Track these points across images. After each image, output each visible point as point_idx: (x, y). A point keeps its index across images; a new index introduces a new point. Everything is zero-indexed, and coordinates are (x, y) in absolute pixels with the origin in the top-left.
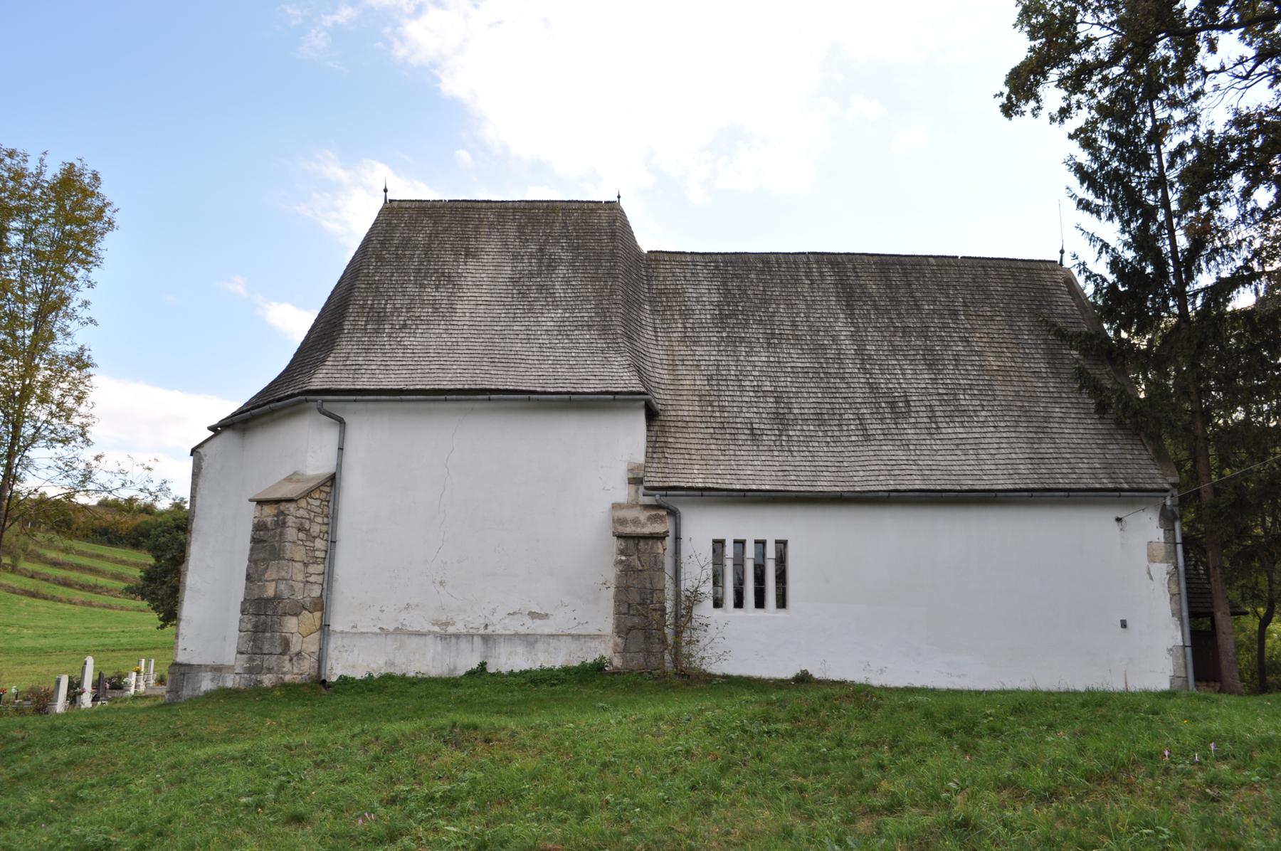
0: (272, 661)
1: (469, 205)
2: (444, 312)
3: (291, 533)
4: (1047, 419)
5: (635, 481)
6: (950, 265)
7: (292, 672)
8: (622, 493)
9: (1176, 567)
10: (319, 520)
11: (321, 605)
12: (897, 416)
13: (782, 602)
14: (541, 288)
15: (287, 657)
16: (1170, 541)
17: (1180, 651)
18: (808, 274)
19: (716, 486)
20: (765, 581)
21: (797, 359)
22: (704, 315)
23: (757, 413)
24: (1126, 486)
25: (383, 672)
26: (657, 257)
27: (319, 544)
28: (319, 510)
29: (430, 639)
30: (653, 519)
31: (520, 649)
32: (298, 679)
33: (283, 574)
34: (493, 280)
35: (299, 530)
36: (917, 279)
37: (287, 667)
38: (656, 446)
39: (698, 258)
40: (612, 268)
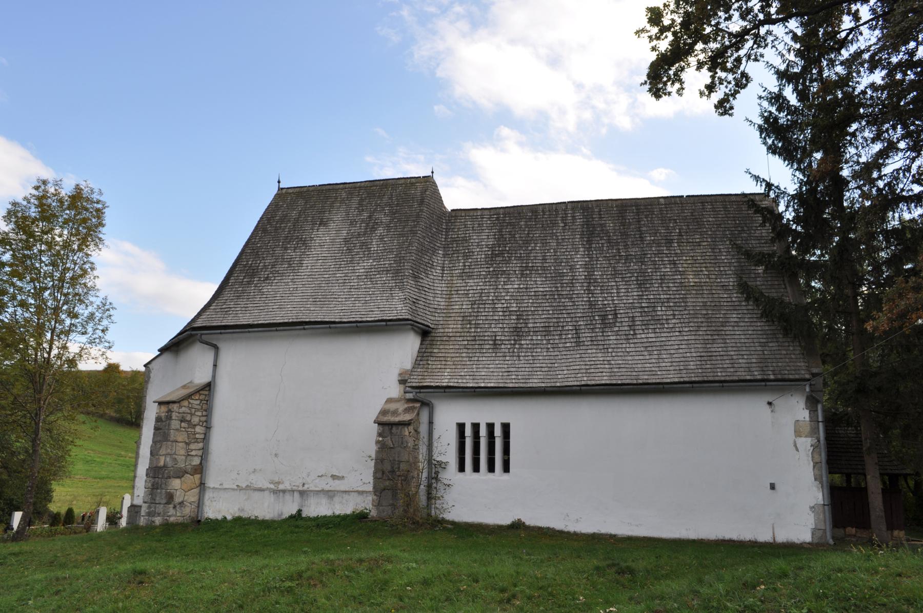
0: (160, 508)
1: (330, 187)
2: (294, 266)
3: (175, 424)
4: (724, 324)
5: (402, 382)
6: (675, 203)
7: (176, 516)
8: (395, 391)
9: (819, 441)
10: (199, 414)
11: (200, 470)
12: (606, 324)
13: (506, 468)
14: (363, 244)
15: (171, 506)
17: (821, 509)
18: (564, 219)
19: (456, 385)
20: (488, 450)
21: (540, 284)
23: (499, 329)
24: (772, 377)
25: (237, 515)
26: (458, 213)
27: (199, 429)
28: (199, 407)
29: (267, 493)
30: (407, 410)
31: (324, 501)
32: (180, 520)
33: (169, 451)
34: (333, 241)
35: (182, 421)
36: (646, 217)
37: (171, 511)
38: (423, 357)
39: (486, 212)
40: (415, 226)
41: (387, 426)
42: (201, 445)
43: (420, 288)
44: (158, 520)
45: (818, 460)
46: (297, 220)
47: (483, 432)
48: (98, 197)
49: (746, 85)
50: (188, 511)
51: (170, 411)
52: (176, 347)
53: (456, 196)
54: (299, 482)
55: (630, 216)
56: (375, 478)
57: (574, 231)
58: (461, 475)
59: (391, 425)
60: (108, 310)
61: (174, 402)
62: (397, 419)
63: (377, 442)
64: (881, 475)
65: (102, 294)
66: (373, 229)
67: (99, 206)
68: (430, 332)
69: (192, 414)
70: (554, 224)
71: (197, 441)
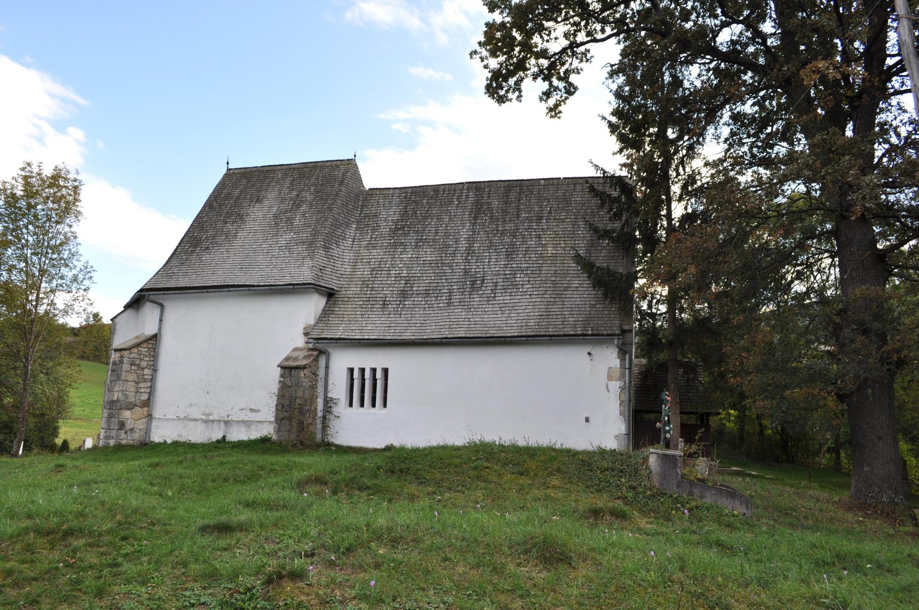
0: (114, 433)
2: (230, 237)
3: (126, 367)
5: (306, 334)
8: (300, 341)
10: (148, 359)
11: (148, 403)
16: (622, 367)
20: (371, 389)
22: (385, 229)
23: (390, 293)
24: (590, 332)
27: (146, 371)
29: (199, 422)
31: (243, 429)
34: (264, 216)
37: (123, 436)
38: (326, 314)
39: (398, 191)
40: (332, 204)
41: (288, 369)
42: (149, 384)
43: (329, 257)
44: (112, 442)
45: (623, 399)
46: (238, 198)
47: (368, 375)
48: (75, 176)
49: (574, 93)
50: (137, 436)
51: (122, 357)
52: (136, 303)
53: (376, 174)
54: (225, 414)
55: (513, 196)
56: (277, 409)
57: (465, 208)
58: (350, 409)
59: (291, 368)
60: (89, 272)
61: (125, 349)
62: (295, 364)
63: (280, 382)
64: (681, 413)
65: (83, 259)
66: (299, 206)
67: (76, 184)
68: (334, 294)
69: (141, 360)
70: (450, 202)
71: (145, 381)
